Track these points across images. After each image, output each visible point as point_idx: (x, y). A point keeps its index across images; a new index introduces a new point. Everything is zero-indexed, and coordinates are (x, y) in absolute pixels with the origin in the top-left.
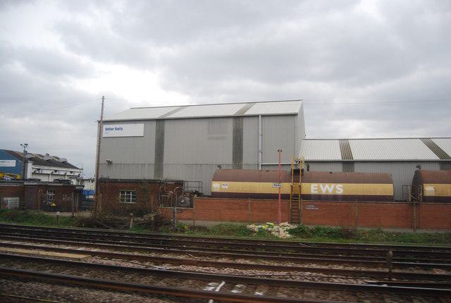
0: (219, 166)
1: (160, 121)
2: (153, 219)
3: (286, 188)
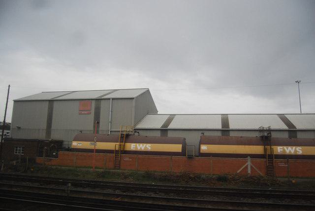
0: (81, 132)
1: (51, 102)
2: (15, 164)
3: (258, 149)
